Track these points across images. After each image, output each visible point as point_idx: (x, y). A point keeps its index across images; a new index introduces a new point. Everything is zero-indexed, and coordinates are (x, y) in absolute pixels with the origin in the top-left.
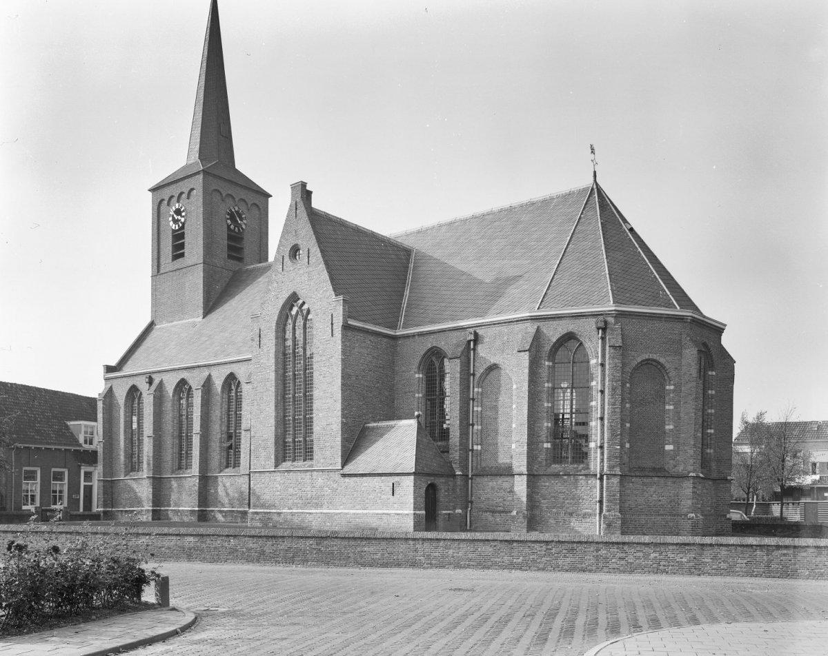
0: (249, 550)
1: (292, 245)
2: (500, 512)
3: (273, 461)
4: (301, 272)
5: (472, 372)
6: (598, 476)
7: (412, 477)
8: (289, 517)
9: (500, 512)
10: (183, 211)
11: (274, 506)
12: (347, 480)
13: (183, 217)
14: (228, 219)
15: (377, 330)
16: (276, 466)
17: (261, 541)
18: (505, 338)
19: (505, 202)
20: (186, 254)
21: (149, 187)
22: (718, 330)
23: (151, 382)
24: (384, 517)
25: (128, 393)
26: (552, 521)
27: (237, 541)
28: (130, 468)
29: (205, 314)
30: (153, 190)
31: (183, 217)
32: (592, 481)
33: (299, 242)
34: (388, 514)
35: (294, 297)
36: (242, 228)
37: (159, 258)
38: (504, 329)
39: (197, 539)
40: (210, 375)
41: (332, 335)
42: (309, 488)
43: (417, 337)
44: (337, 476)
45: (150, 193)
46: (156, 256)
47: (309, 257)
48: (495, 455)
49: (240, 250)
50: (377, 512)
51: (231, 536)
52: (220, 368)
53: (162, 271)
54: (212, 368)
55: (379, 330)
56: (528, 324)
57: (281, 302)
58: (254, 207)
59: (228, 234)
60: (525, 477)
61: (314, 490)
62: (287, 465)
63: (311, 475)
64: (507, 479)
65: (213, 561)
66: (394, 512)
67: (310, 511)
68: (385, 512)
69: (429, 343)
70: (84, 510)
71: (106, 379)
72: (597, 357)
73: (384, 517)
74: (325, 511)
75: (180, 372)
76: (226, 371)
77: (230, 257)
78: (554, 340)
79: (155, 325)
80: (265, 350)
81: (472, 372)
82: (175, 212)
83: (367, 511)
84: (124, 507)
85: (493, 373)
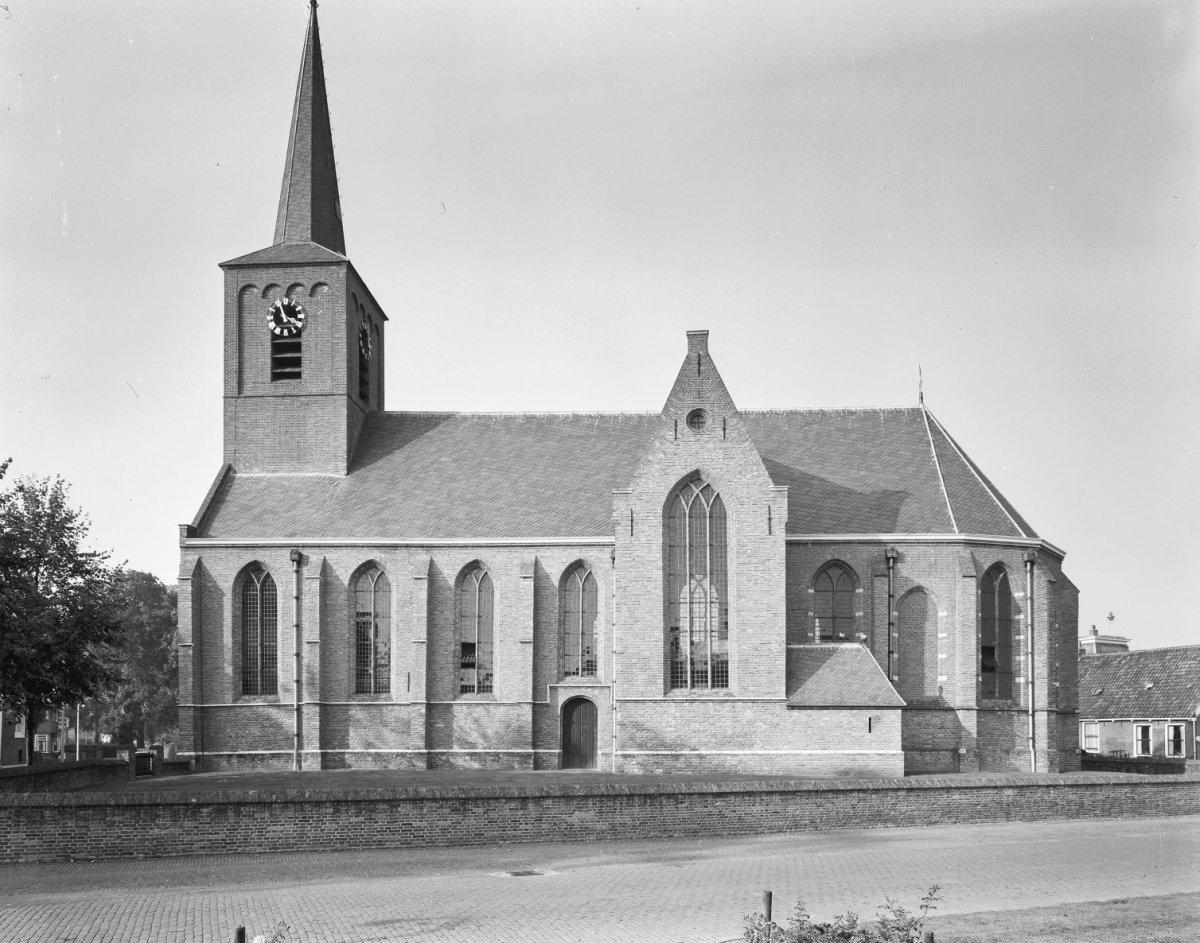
0: (1069, 802)
1: (691, 409)
2: (930, 750)
3: (662, 686)
4: (711, 446)
6: (1030, 712)
7: (899, 711)
8: (696, 761)
9: (930, 750)
11: (683, 746)
12: (795, 713)
13: (300, 320)
16: (665, 694)
17: (1080, 791)
18: (932, 559)
19: (803, 404)
20: (303, 376)
21: (230, 256)
23: (300, 561)
24: (859, 758)
25: (240, 573)
26: (990, 759)
27: (1057, 792)
28: (241, 689)
29: (351, 469)
30: (227, 267)
31: (300, 320)
32: (1023, 717)
33: (707, 407)
34: (864, 755)
35: (694, 477)
37: (240, 372)
38: (931, 550)
39: (1016, 791)
40: (325, 560)
41: (770, 533)
42: (728, 723)
43: (810, 546)
44: (780, 709)
45: (221, 272)
47: (724, 429)
48: (922, 689)
50: (847, 752)
51: (1051, 786)
52: (454, 552)
53: (246, 392)
54: (435, 551)
55: (988, 539)
56: (960, 548)
57: (673, 480)
60: (975, 712)
61: (736, 725)
62: (678, 693)
63: (734, 707)
64: (936, 714)
65: (1033, 819)
66: (872, 752)
67: (733, 752)
68: (860, 752)
69: (829, 555)
70: (1140, 751)
71: (185, 548)
72: (1025, 590)
73: (859, 758)
74: (759, 752)
75: (365, 550)
78: (986, 568)
79: (235, 472)
80: (643, 540)
83: (828, 752)
84: (234, 748)
85: (915, 596)
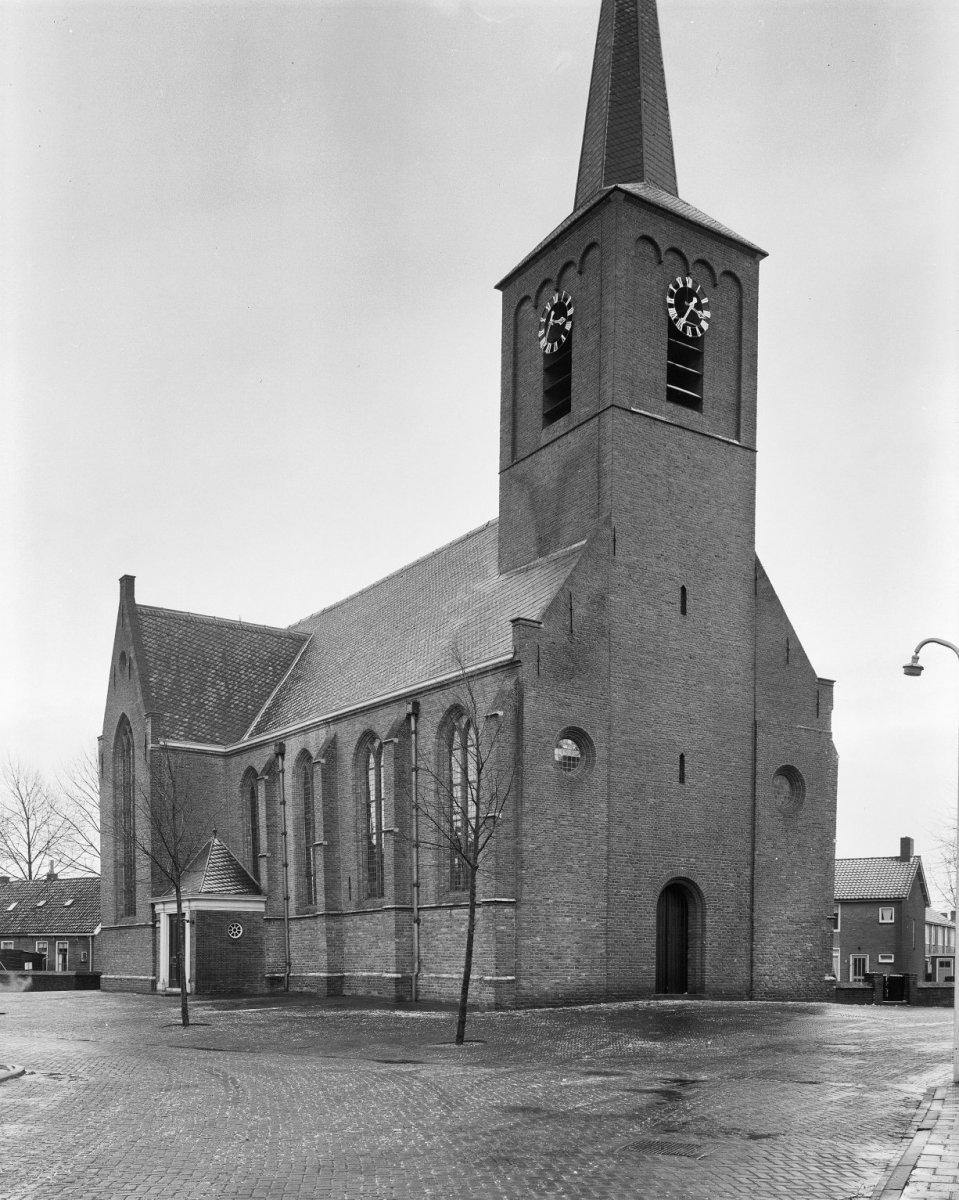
5: (413, 729)
10: (570, 306)
13: (570, 318)
14: (671, 306)
15: (188, 746)
22: (100, 739)
36: (702, 330)
45: (499, 293)
46: (509, 404)
49: (694, 381)
58: (729, 280)
59: (670, 343)
76: (359, 726)
77: (673, 397)
81: (413, 729)
82: (554, 308)
